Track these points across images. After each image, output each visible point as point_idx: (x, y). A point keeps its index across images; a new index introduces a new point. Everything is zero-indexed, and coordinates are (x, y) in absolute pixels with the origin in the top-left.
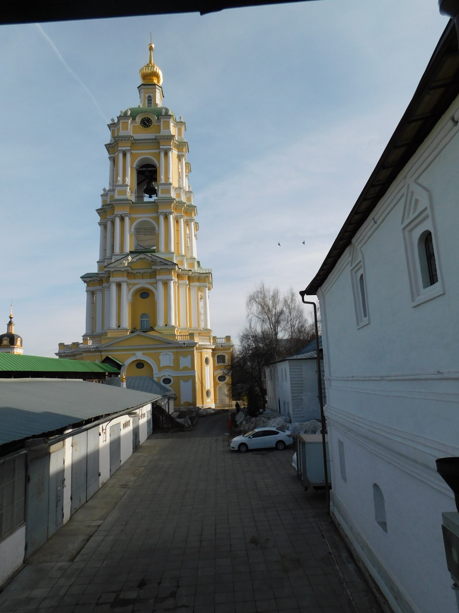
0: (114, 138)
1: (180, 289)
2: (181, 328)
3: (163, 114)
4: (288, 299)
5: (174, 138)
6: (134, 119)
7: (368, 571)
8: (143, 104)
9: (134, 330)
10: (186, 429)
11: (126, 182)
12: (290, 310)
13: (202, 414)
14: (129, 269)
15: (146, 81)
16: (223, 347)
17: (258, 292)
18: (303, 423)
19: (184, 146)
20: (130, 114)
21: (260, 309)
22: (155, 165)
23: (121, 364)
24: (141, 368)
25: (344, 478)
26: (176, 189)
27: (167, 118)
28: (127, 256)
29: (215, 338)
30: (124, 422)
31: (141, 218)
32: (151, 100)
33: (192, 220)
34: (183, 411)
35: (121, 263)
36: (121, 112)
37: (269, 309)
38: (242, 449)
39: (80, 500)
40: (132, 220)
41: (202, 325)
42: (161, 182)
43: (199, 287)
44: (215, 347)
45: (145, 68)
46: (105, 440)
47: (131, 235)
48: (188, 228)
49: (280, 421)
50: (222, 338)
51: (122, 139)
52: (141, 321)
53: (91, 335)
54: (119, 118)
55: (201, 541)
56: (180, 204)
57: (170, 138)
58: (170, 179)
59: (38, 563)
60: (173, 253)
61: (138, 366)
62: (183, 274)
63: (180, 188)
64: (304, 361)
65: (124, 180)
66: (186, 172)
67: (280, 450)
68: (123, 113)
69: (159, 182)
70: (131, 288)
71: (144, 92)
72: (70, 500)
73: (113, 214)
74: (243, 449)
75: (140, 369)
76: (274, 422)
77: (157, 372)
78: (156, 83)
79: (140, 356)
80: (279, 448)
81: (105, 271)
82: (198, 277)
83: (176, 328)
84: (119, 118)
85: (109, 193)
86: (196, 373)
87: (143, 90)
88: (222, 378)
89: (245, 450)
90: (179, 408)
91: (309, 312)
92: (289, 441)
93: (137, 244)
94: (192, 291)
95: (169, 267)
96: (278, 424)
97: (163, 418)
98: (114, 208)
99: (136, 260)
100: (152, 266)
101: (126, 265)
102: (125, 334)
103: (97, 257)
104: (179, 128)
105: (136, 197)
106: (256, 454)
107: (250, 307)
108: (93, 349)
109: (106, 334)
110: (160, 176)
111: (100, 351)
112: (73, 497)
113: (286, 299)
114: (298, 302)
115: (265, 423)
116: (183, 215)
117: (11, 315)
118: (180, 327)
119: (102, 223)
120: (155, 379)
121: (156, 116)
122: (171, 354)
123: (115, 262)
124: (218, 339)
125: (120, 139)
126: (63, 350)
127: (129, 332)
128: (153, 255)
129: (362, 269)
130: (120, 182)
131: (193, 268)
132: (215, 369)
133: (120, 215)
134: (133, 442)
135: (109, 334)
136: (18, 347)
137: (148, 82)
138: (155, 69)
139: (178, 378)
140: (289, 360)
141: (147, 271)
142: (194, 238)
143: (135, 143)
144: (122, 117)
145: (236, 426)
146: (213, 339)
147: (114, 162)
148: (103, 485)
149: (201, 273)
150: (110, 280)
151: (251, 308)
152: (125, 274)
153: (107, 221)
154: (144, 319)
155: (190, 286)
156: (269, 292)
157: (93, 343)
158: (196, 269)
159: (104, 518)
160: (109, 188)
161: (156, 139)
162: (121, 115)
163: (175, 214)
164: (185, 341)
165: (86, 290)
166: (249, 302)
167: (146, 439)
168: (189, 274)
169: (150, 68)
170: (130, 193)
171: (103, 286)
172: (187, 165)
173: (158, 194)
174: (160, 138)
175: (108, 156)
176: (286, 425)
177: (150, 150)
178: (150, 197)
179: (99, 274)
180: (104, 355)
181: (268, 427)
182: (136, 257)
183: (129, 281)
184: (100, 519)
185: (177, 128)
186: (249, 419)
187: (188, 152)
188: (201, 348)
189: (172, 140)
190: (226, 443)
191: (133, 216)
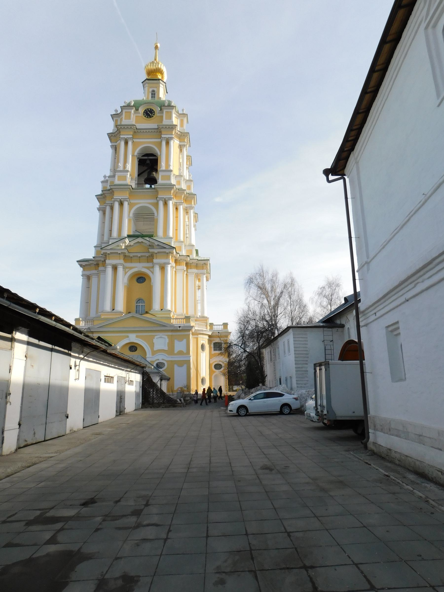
1: (177, 275)
5: (175, 128)
6: (137, 110)
8: (146, 97)
11: (127, 168)
14: (126, 251)
22: (155, 154)
24: (134, 352)
26: (176, 176)
29: (211, 325)
32: (155, 94)
35: (118, 246)
42: (161, 169)
43: (197, 274)
46: (78, 378)
47: (129, 221)
51: (124, 128)
52: (136, 305)
55: (189, 468)
60: (172, 238)
63: (180, 176)
65: (125, 166)
66: (187, 164)
71: (148, 86)
73: (112, 199)
75: (133, 352)
77: (151, 356)
78: (160, 78)
79: (133, 338)
83: (172, 312)
87: (147, 85)
92: (295, 405)
95: (167, 251)
100: (149, 249)
104: (181, 120)
105: (136, 184)
119: (101, 209)
122: (166, 337)
125: (123, 127)
133: (119, 200)
138: (159, 66)
139: (172, 363)
141: (145, 255)
142: (193, 229)
143: (137, 132)
146: (210, 326)
147: (116, 150)
152: (122, 256)
153: (106, 206)
155: (188, 272)
158: (194, 256)
163: (175, 200)
164: (181, 324)
169: (155, 64)
170: (130, 180)
171: (99, 270)
174: (162, 128)
175: (110, 144)
188: (197, 334)
189: (174, 129)
191: (132, 201)
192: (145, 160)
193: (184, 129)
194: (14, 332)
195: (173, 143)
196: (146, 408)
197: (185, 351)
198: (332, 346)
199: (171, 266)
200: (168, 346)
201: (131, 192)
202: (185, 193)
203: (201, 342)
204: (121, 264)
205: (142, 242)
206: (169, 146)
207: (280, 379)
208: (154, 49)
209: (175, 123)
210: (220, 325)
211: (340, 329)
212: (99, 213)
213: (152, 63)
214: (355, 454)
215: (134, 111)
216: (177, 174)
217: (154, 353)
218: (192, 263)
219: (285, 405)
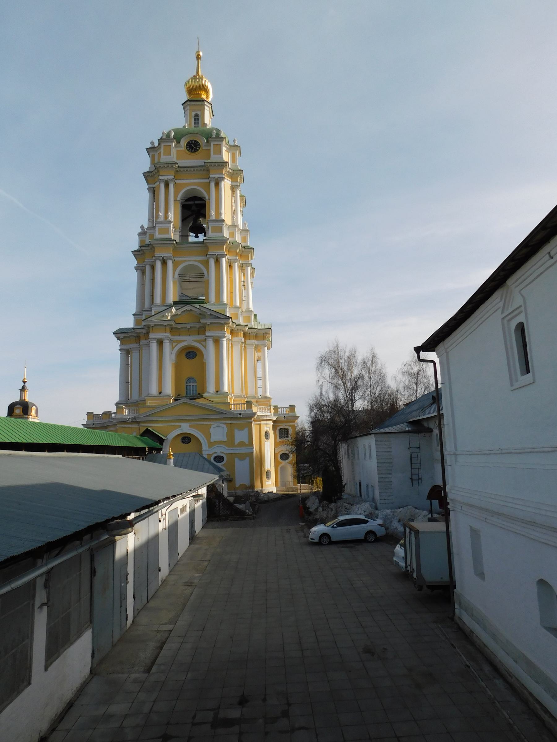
2: (235, 395)
3: (214, 136)
6: (178, 142)
7: (526, 688)
8: (189, 124)
9: (178, 397)
10: (248, 517)
11: (169, 218)
12: (370, 373)
13: (262, 499)
14: (173, 323)
16: (286, 418)
17: (330, 351)
18: (396, 510)
19: (239, 175)
20: (173, 136)
21: (333, 372)
22: (203, 198)
23: (164, 438)
24: (187, 443)
27: (217, 141)
28: (171, 307)
29: (276, 407)
31: (185, 261)
32: (198, 119)
33: (249, 265)
34: (239, 496)
35: (163, 316)
36: (163, 133)
38: (323, 541)
39: (142, 599)
40: (176, 264)
41: (260, 392)
42: (211, 219)
45: (191, 80)
47: (174, 282)
48: (242, 273)
49: (367, 507)
50: (283, 408)
52: (186, 386)
53: (125, 402)
57: (222, 165)
58: (222, 215)
59: (107, 674)
60: (226, 304)
61: (184, 440)
62: (238, 330)
64: (394, 435)
65: (166, 216)
68: (165, 135)
69: (209, 218)
71: (190, 110)
72: (133, 599)
73: (153, 257)
74: (325, 541)
76: (360, 509)
77: (207, 449)
78: (204, 99)
79: (186, 428)
80: (323, 542)
81: (143, 326)
82: (255, 334)
83: (230, 395)
84: (161, 140)
88: (284, 457)
89: (327, 542)
90: (235, 492)
91: (392, 376)
92: (381, 532)
93: (182, 293)
97: (219, 504)
98: (155, 249)
99: (181, 312)
100: (200, 320)
101: (169, 318)
102: (168, 402)
103: (133, 307)
104: (232, 153)
107: (320, 370)
108: (130, 420)
109: (144, 401)
111: (138, 422)
112: (136, 596)
113: (365, 360)
114: (380, 364)
115: (347, 510)
116: (238, 258)
117: (24, 378)
118: (234, 395)
119: (140, 268)
120: (205, 455)
121: (205, 139)
122: (225, 426)
123: (155, 315)
125: (162, 166)
126: (92, 421)
127: (173, 400)
128: (203, 307)
132: (276, 445)
133: (161, 258)
134: (189, 532)
135: (149, 402)
136: (32, 417)
137: (194, 97)
138: (203, 82)
139: (232, 456)
143: (180, 171)
144: (164, 139)
145: (310, 513)
146: (274, 409)
147: (154, 193)
148: (162, 582)
149: (259, 329)
150: (150, 336)
151: (322, 371)
152: (168, 329)
153: (146, 265)
154: (190, 384)
155: (246, 344)
156: (345, 352)
158: (253, 324)
159: (174, 621)
160: (148, 225)
161: (205, 166)
162: (163, 137)
164: (242, 410)
165: (119, 349)
166: (320, 364)
167: (202, 529)
169: (197, 80)
171: (141, 344)
172: (242, 198)
173: (208, 233)
175: (147, 186)
176: (375, 512)
177: (203, 179)
178: (197, 236)
180: (143, 427)
183: (172, 338)
184: (170, 623)
185: (230, 153)
187: (243, 182)
189: (224, 167)
190: (301, 534)
191: (176, 259)
193: (237, 165)
194: (127, 517)
198: (419, 454)
199: (227, 339)
201: (175, 247)
204: (168, 338)
205: (191, 310)
206: (220, 189)
207: (360, 484)
208: (195, 59)
211: (428, 434)
212: (136, 273)
214: (442, 629)
217: (211, 444)
218: (251, 332)
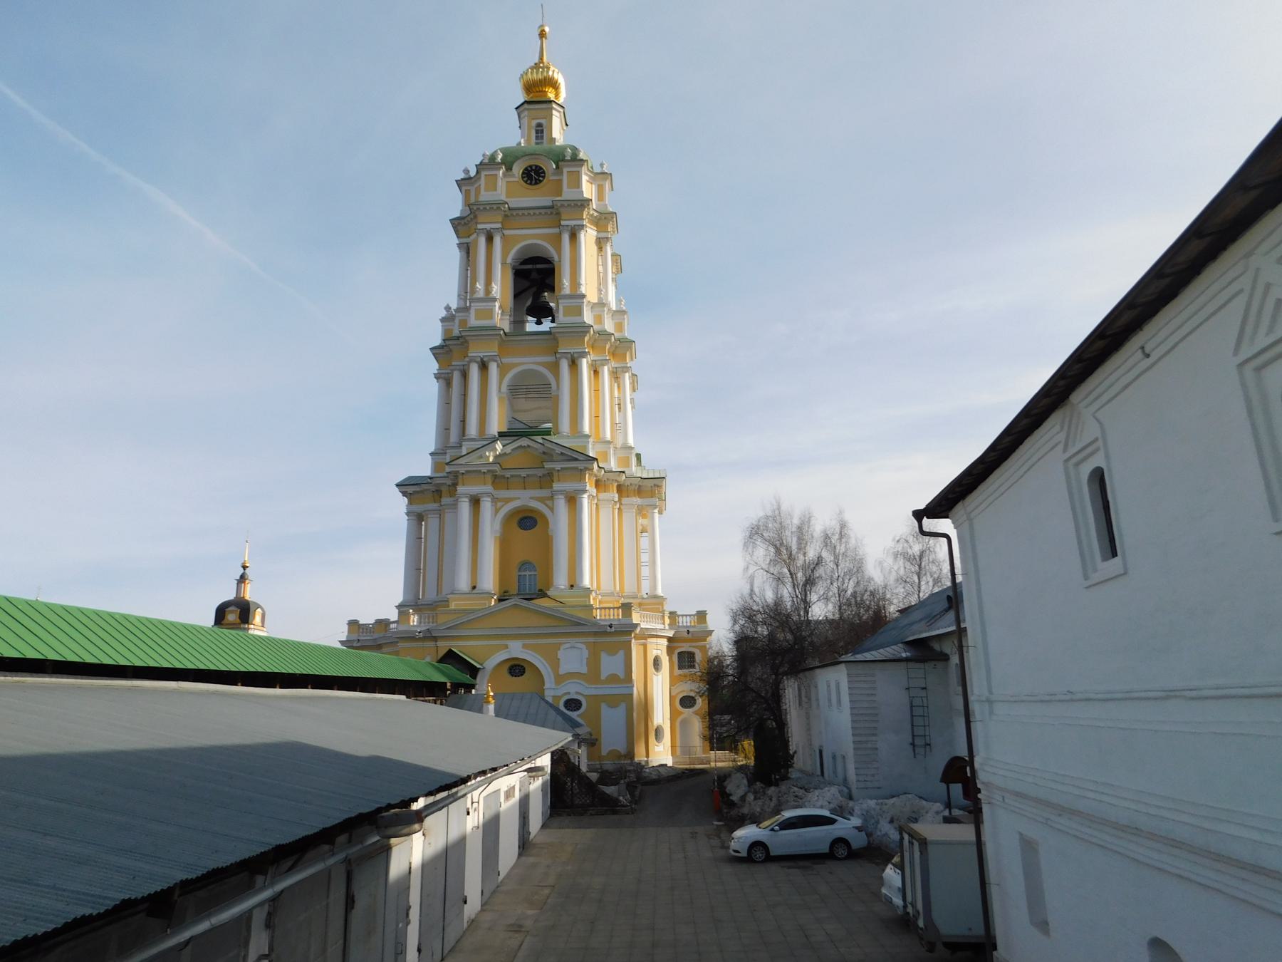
0: (469, 205)
4: (833, 534)
5: (589, 205)
6: (509, 169)
8: (526, 138)
9: (504, 596)
11: (493, 293)
14: (497, 468)
15: (531, 95)
17: (767, 517)
23: (478, 666)
25: (1043, 926)
26: (594, 306)
28: (495, 441)
29: (673, 615)
30: (506, 789)
34: (607, 771)
35: (481, 457)
36: (484, 155)
37: (791, 554)
40: (503, 370)
42: (563, 293)
44: (674, 635)
47: (500, 399)
48: (616, 385)
54: (478, 167)
56: (602, 337)
60: (588, 436)
62: (608, 479)
67: (840, 859)
68: (488, 157)
70: (500, 508)
72: (417, 954)
73: (465, 357)
74: (759, 855)
77: (553, 686)
78: (552, 99)
79: (516, 650)
83: (593, 593)
84: (481, 167)
85: (457, 315)
86: (635, 689)
87: (526, 113)
92: (858, 841)
94: (625, 516)
96: (829, 803)
100: (544, 463)
104: (599, 185)
106: (789, 868)
107: (750, 550)
109: (446, 602)
110: (561, 281)
111: (435, 639)
116: (608, 358)
119: (443, 376)
122: (583, 646)
124: (680, 618)
129: (1101, 454)
130: (481, 294)
131: (629, 467)
133: (479, 359)
134: (519, 834)
136: (256, 627)
138: (551, 73)
140: (847, 664)
143: (511, 215)
144: (486, 164)
146: (669, 617)
147: (468, 253)
152: (489, 478)
153: (452, 371)
157: (420, 622)
158: (634, 470)
160: (458, 304)
161: (552, 207)
164: (614, 620)
168: (620, 480)
170: (499, 316)
174: (562, 206)
177: (543, 228)
178: (539, 323)
179: (435, 479)
180: (444, 647)
181: (805, 807)
182: (510, 445)
186: (761, 790)
188: (647, 635)
190: (716, 842)
192: (529, 271)
195: (585, 235)
196: (559, 815)
197: (622, 676)
198: (925, 700)
199: (589, 496)
200: (587, 665)
202: (613, 340)
203: (652, 653)
204: (488, 494)
205: (529, 446)
209: (587, 195)
210: (690, 616)
211: (940, 665)
213: (535, 68)
215: (503, 173)
216: (595, 300)
217: (559, 679)
219: (840, 841)
